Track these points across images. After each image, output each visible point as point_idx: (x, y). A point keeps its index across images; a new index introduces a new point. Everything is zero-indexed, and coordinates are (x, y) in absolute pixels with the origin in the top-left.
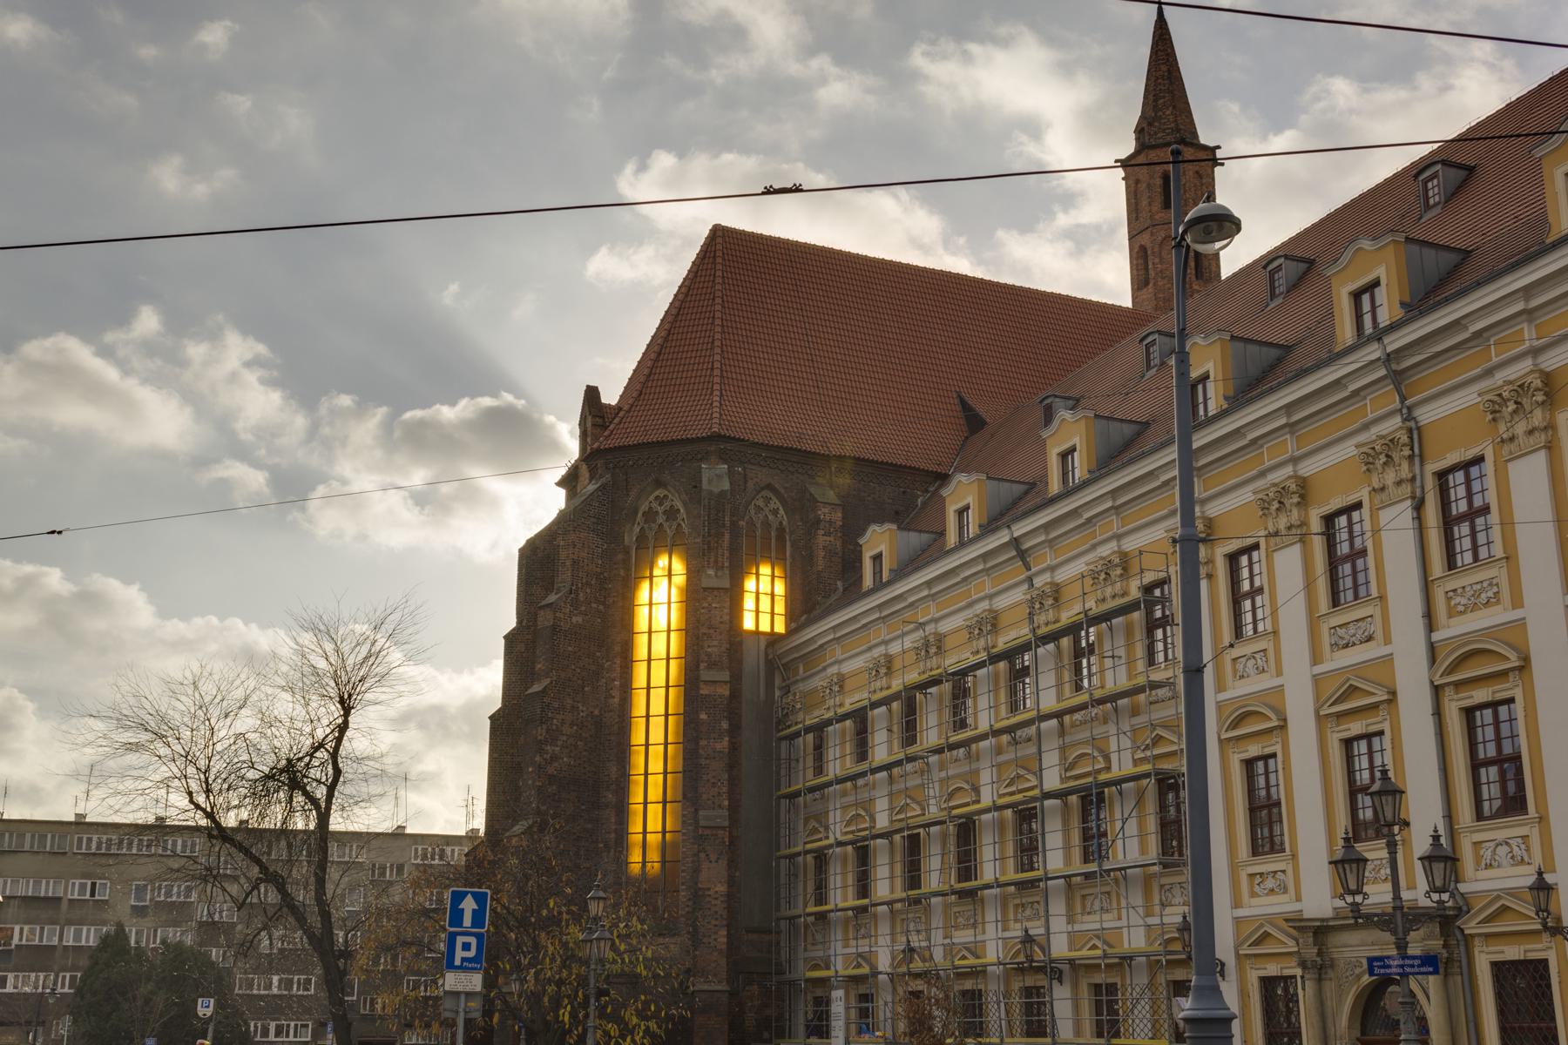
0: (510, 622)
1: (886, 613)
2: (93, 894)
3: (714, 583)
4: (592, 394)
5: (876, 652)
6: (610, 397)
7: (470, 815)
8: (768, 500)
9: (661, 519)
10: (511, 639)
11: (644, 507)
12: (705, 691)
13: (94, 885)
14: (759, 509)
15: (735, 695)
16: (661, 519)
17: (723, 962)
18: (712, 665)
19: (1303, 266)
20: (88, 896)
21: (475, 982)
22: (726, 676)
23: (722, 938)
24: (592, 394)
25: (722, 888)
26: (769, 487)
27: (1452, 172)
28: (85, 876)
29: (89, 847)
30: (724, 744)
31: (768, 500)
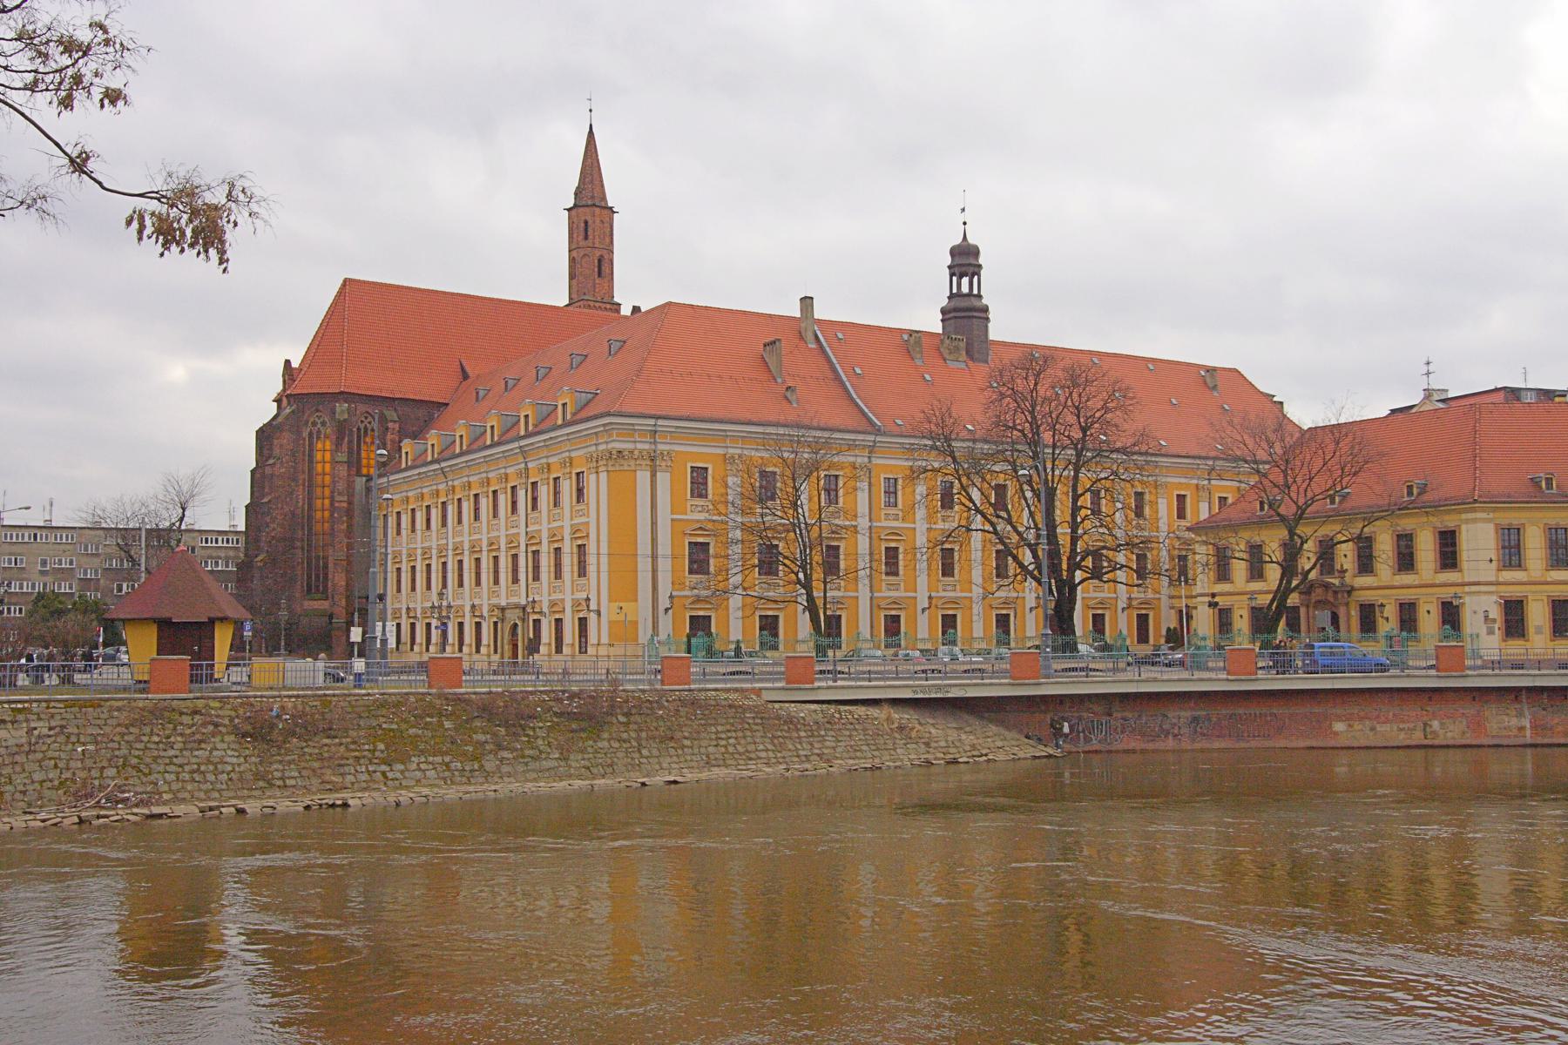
0: (248, 501)
1: (407, 481)
2: (16, 564)
3: (340, 459)
4: (287, 363)
5: (564, 455)
6: (295, 364)
7: (232, 517)
8: (366, 418)
9: (319, 426)
10: (253, 472)
11: (312, 420)
12: (337, 505)
13: (16, 559)
14: (362, 422)
15: (350, 503)
16: (319, 426)
17: (344, 611)
18: (340, 494)
19: (583, 358)
20: (13, 565)
21: (250, 634)
22: (345, 498)
23: (343, 603)
24: (287, 363)
25: (344, 583)
26: (367, 412)
27: (618, 343)
28: (10, 554)
29: (67, 539)
30: (344, 526)
31: (366, 418)
